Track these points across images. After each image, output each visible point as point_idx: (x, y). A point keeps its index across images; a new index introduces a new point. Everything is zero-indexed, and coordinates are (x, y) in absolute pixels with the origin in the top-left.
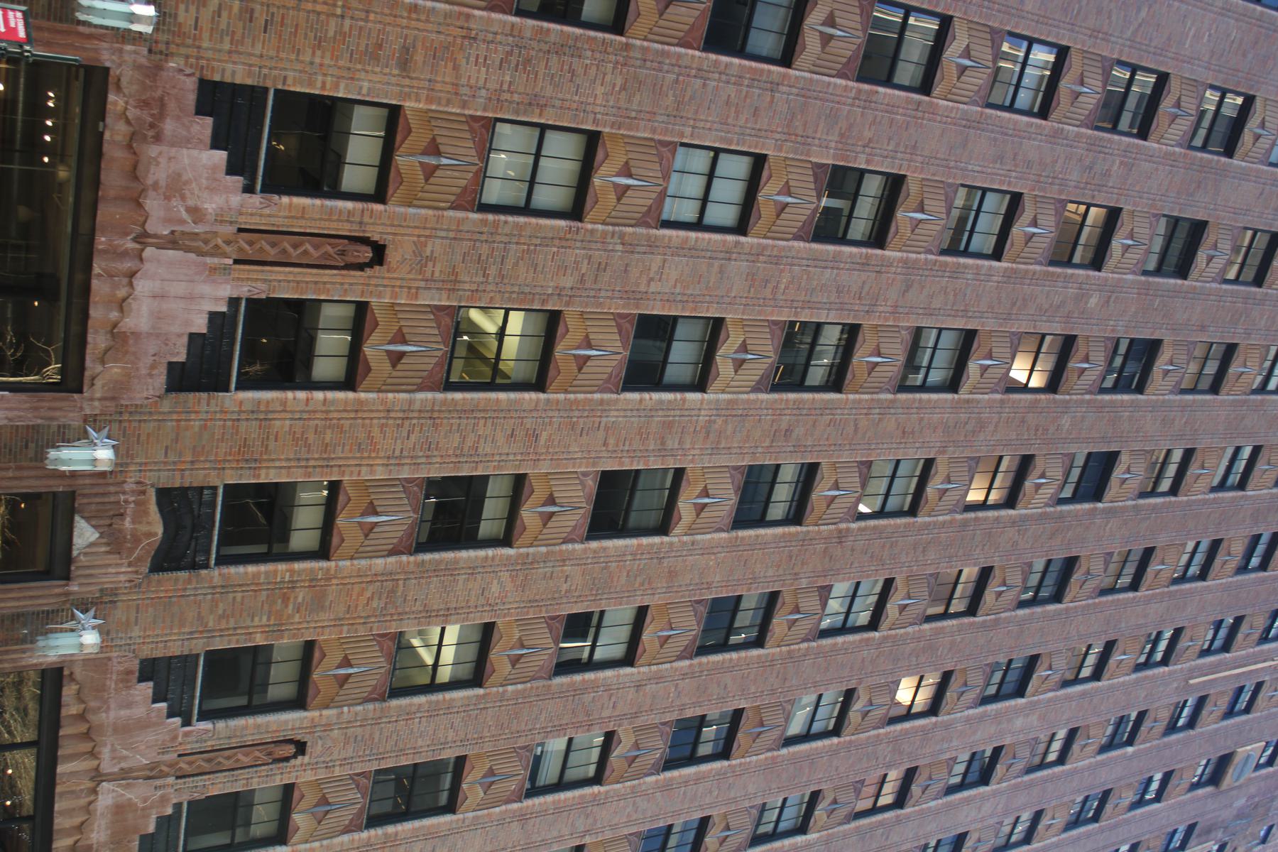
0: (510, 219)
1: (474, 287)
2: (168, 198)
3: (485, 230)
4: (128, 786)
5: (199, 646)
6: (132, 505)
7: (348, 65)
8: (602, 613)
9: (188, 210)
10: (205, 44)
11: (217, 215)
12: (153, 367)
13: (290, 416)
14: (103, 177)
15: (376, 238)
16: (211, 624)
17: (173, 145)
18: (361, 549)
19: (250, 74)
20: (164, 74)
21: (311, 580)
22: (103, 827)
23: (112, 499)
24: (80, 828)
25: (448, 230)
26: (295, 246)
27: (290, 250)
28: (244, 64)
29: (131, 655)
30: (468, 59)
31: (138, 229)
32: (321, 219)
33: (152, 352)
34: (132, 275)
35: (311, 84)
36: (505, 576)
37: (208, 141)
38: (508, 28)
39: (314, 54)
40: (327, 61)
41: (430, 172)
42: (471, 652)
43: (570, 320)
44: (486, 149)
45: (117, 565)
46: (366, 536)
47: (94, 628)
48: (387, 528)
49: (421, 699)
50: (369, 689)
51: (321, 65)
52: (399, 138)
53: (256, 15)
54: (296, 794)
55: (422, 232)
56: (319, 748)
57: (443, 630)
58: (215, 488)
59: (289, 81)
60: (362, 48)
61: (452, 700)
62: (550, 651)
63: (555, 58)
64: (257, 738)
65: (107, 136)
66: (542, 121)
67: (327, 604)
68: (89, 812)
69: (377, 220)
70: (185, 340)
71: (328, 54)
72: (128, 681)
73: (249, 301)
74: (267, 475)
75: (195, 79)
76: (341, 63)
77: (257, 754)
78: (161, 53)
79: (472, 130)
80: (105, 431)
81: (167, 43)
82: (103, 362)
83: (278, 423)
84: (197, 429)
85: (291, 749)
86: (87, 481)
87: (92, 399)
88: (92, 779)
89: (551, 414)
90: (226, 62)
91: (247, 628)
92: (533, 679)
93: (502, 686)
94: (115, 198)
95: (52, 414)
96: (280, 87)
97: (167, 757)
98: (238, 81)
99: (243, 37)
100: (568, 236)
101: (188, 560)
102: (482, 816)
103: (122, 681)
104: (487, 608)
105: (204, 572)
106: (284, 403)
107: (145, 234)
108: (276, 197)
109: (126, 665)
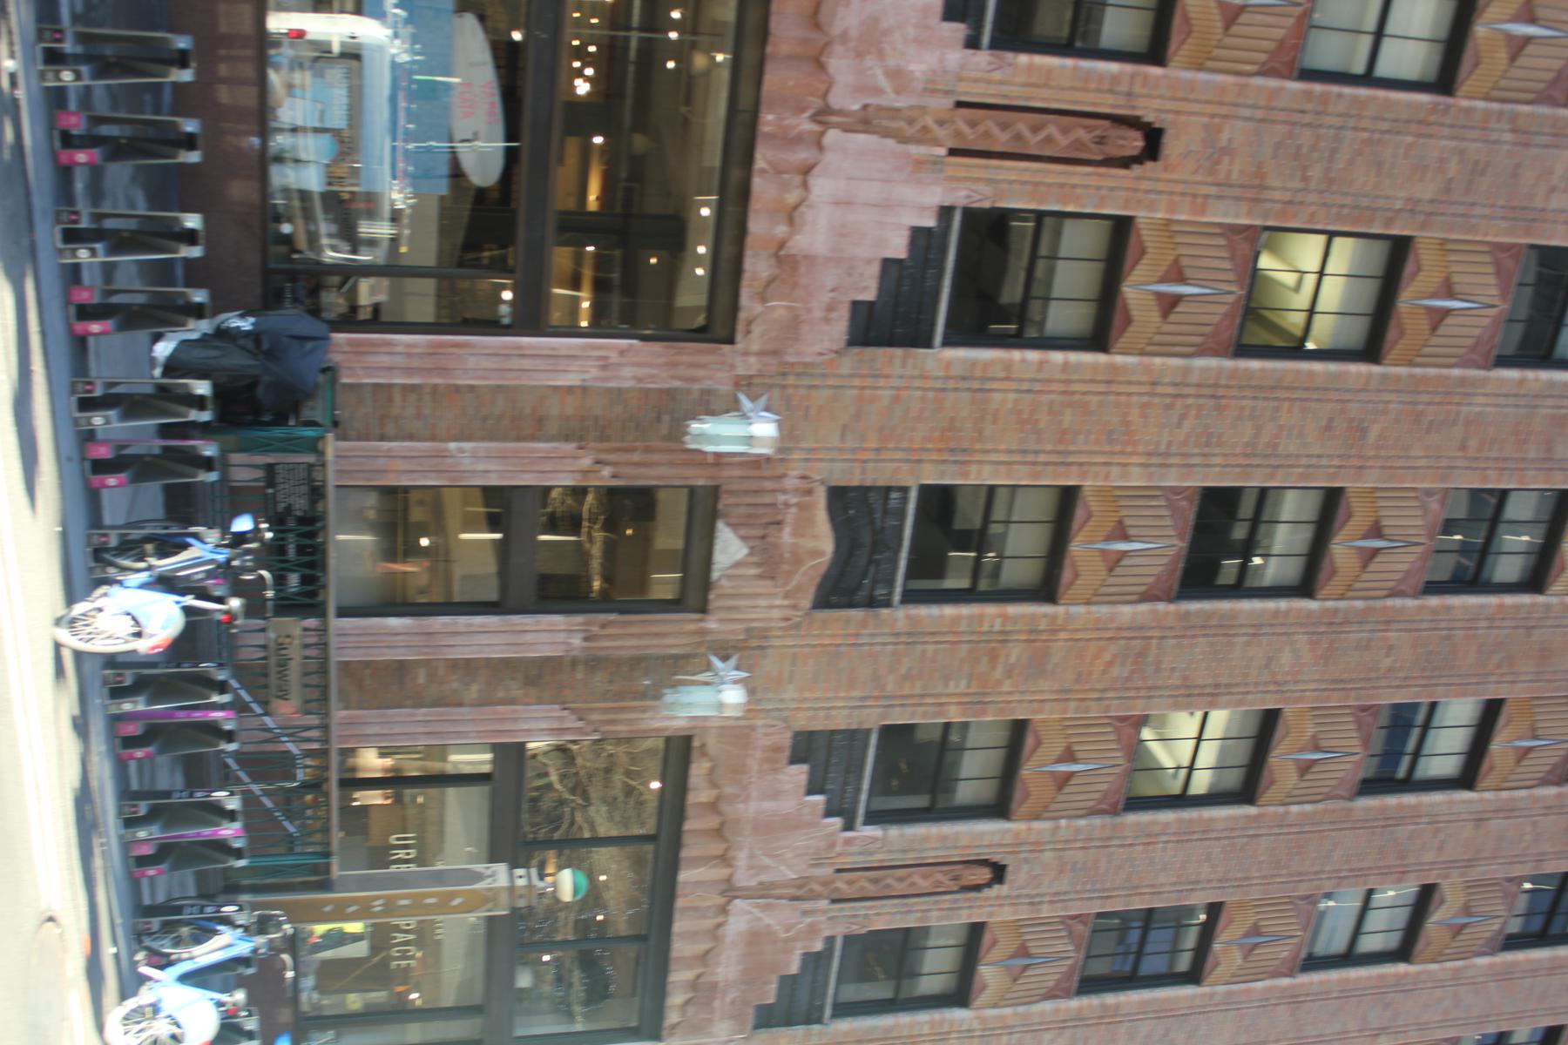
26: (1035, 129)
29: (781, 724)
77: (940, 877)
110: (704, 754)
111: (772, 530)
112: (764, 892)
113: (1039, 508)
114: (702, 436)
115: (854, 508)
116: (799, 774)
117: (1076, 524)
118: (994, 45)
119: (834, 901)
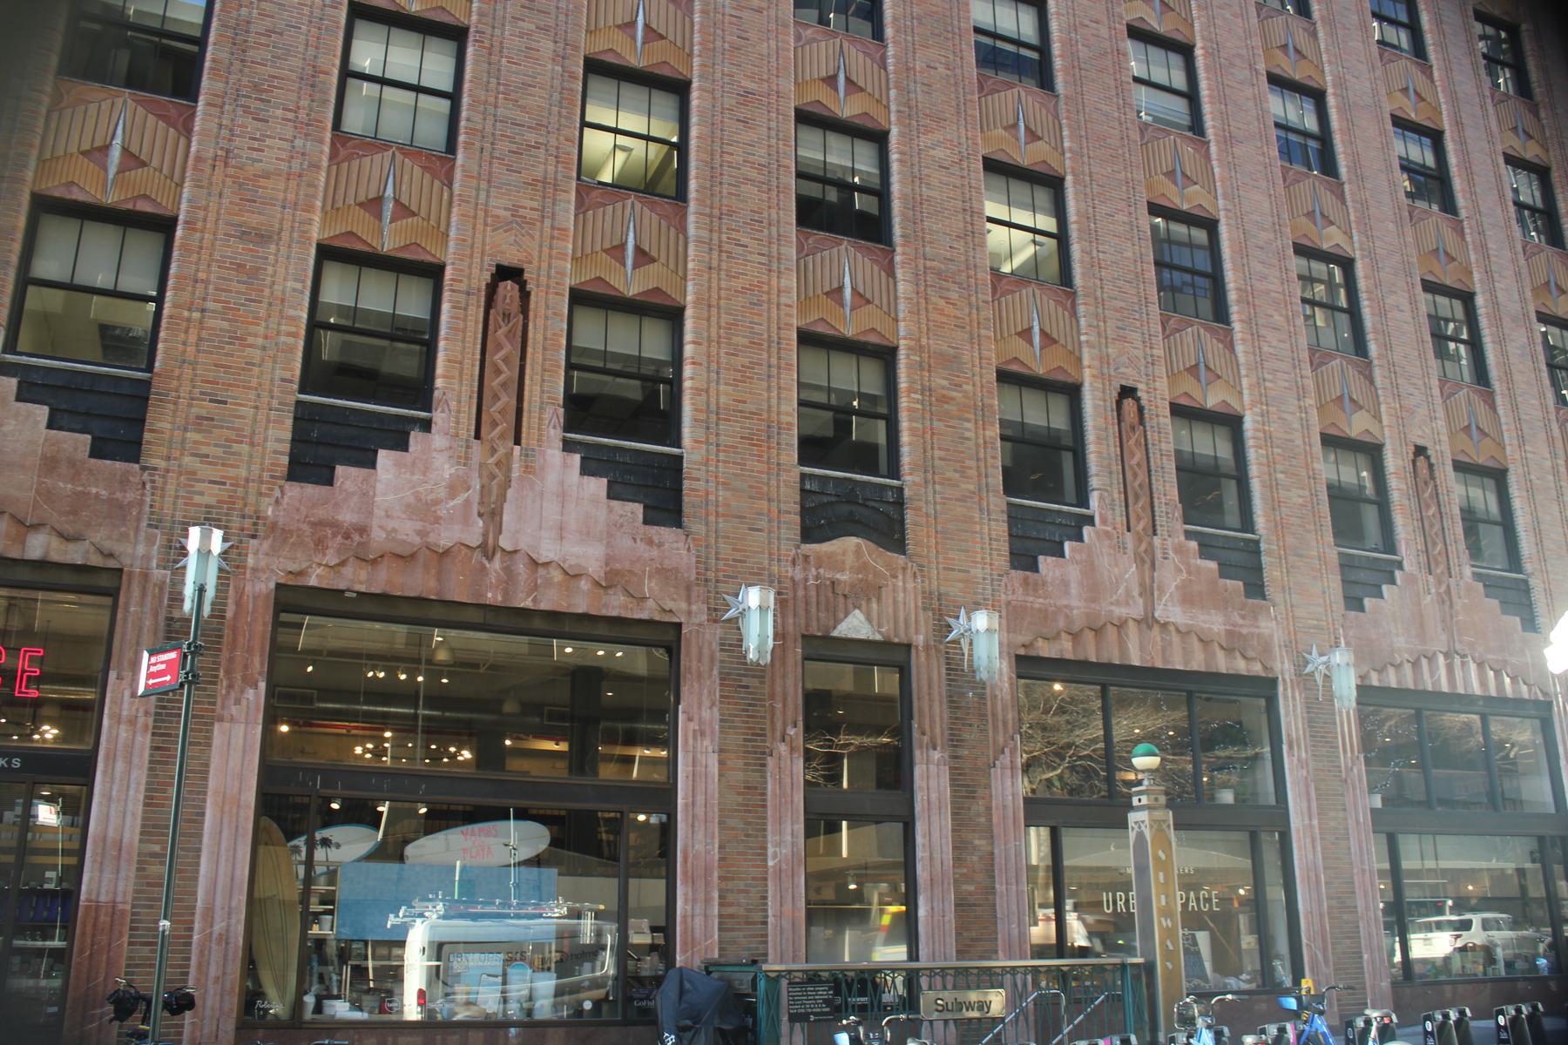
0: (464, 114)
1: (552, 160)
2: (437, 520)
3: (478, 145)
4: (1161, 589)
5: (998, 502)
6: (821, 571)
7: (264, 305)
8: (977, 30)
9: (452, 496)
10: (243, 473)
11: (459, 463)
12: (650, 542)
13: (713, 385)
14: (412, 594)
15: (487, 277)
16: (972, 487)
17: (371, 513)
18: (885, 308)
19: (279, 422)
20: (281, 521)
21: (922, 369)
22: (1206, 617)
23: (813, 593)
24: (1205, 642)
25: (478, 189)
26: (498, 372)
27: (502, 378)
28: (266, 429)
29: (1004, 579)
30: (255, 160)
31: (477, 555)
32: (463, 341)
33: (630, 543)
34: (534, 563)
35: (291, 349)
36: (924, 140)
37: (365, 471)
38: (213, 110)
39: (250, 346)
40: (261, 330)
41: (403, 211)
42: (1020, 189)
43: (598, 46)
44: (374, 143)
45: (894, 591)
46: (868, 302)
47: (969, 619)
48: (860, 277)
49: (1076, 250)
50: (1060, 309)
51: (266, 337)
52: (360, 247)
53: (204, 413)
54: (1183, 401)
55: (480, 221)
56: (1129, 371)
57: (991, 220)
58: (803, 476)
59: (288, 375)
60: (243, 288)
61: (1078, 213)
62: (1023, 94)
63: (251, 53)
64: (1113, 441)
65: (363, 588)
66: (336, 72)
67: (952, 351)
68: (1188, 633)
69: (465, 275)
70: (615, 503)
71: (252, 329)
72: (1036, 584)
73: (567, 429)
74: (788, 414)
75: (288, 485)
76: (262, 313)
77: (1132, 442)
78: (255, 524)
79: (349, 158)
81: (243, 517)
82: (644, 599)
83: (723, 399)
84: (728, 494)
85: (1129, 403)
86: (791, 621)
87: (689, 613)
88: (1150, 628)
89: (718, 75)
90: (264, 449)
91: (977, 445)
92: (1056, 117)
93: (1063, 154)
94: (439, 580)
95: (706, 660)
96: (296, 387)
97: (1130, 546)
98: (289, 436)
99: (233, 429)
100: (487, 44)
101: (891, 510)
102: (1223, 187)
103: (1035, 590)
104: (965, 165)
105: (907, 492)
106: (697, 391)
107: (483, 547)
108: (436, 394)
109: (1017, 585)
116: (346, 475)
117: (832, 332)
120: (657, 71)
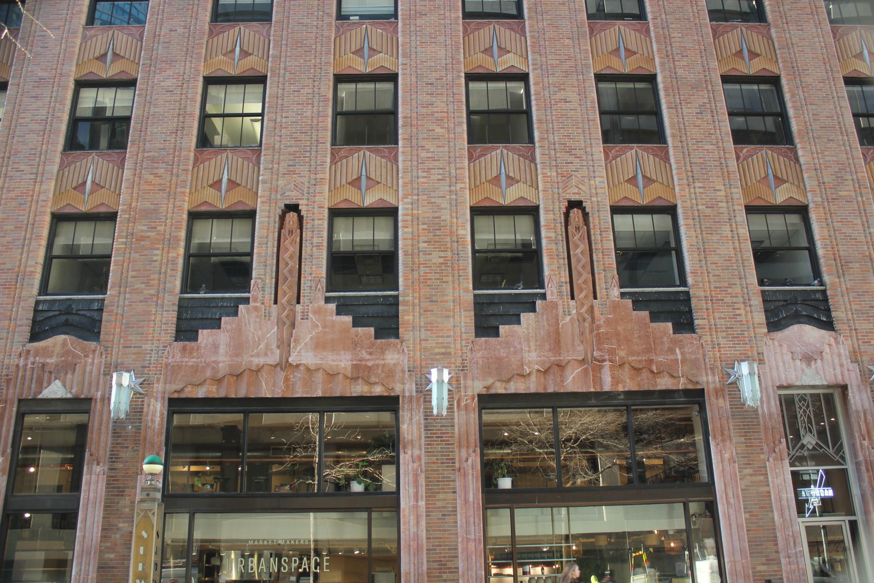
6: (37, 358)
18: (665, 183)
22: (335, 357)
26: (287, 264)
29: (168, 349)
80: (730, 371)
103: (191, 353)
110: (182, 390)
111: (47, 369)
112: (285, 345)
113: (760, 223)
114: (439, 407)
115: (778, 316)
116: (204, 335)
117: (74, 211)
118: (542, 286)
119: (298, 302)
120: (116, 78)
